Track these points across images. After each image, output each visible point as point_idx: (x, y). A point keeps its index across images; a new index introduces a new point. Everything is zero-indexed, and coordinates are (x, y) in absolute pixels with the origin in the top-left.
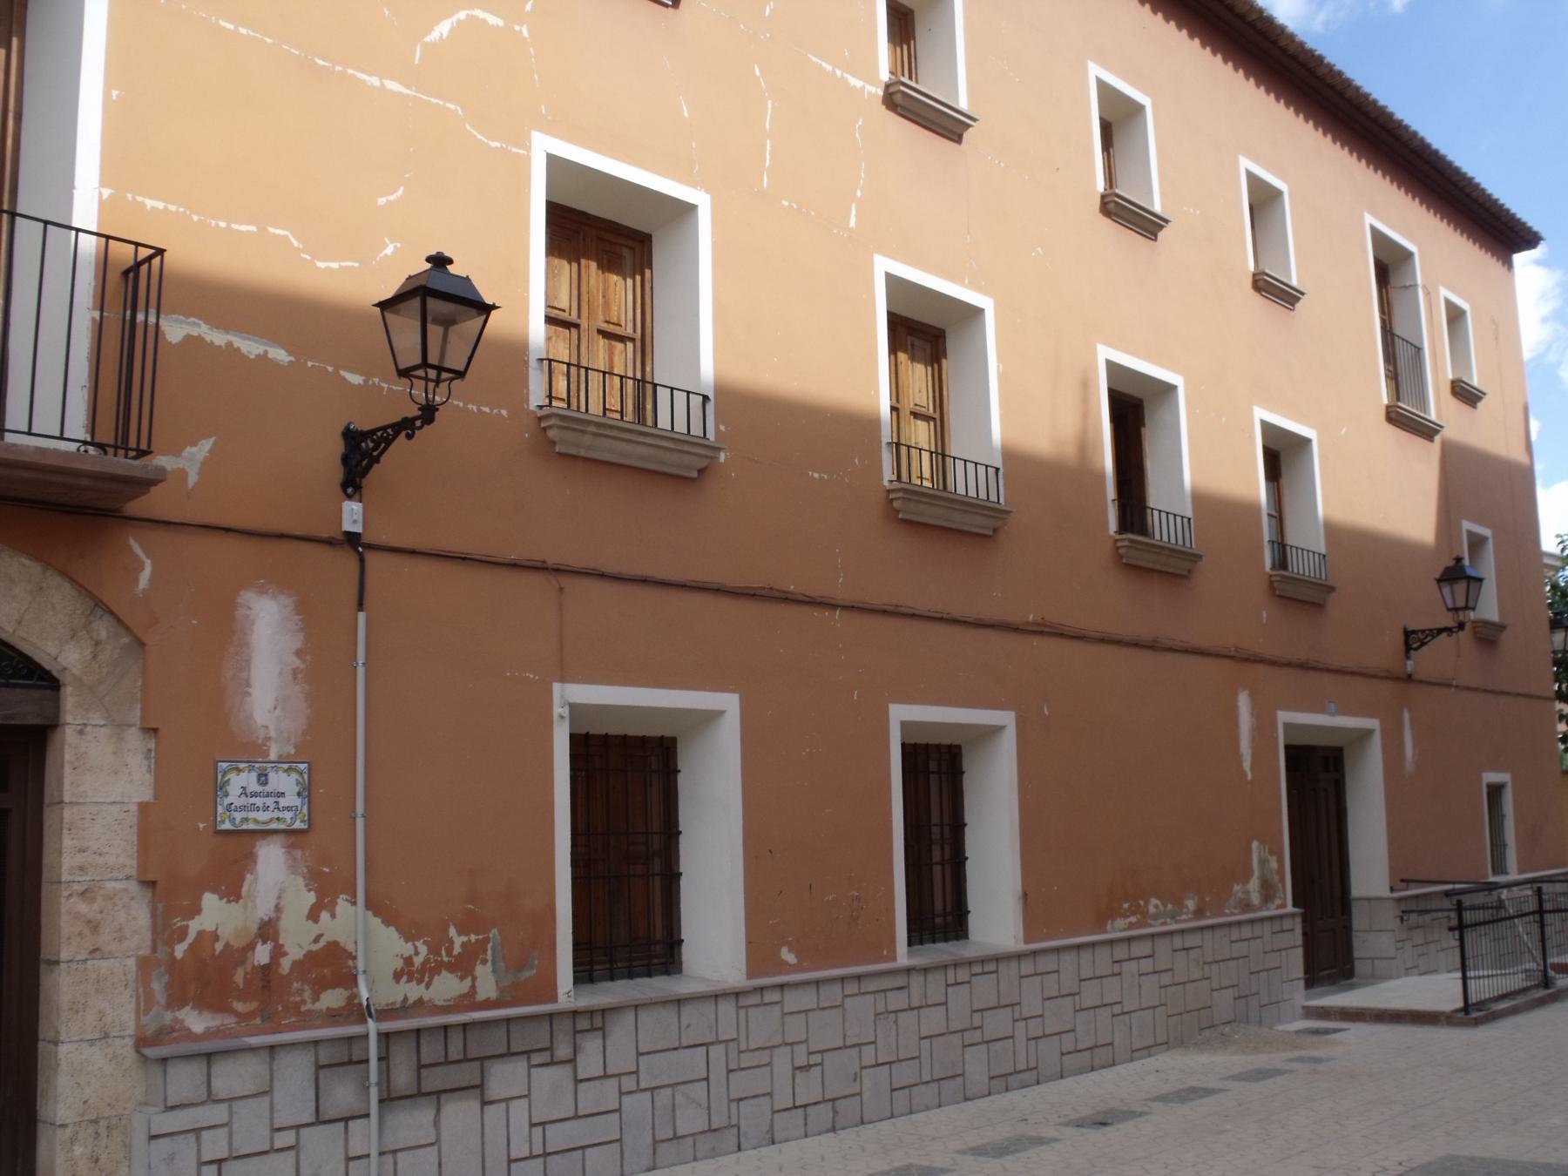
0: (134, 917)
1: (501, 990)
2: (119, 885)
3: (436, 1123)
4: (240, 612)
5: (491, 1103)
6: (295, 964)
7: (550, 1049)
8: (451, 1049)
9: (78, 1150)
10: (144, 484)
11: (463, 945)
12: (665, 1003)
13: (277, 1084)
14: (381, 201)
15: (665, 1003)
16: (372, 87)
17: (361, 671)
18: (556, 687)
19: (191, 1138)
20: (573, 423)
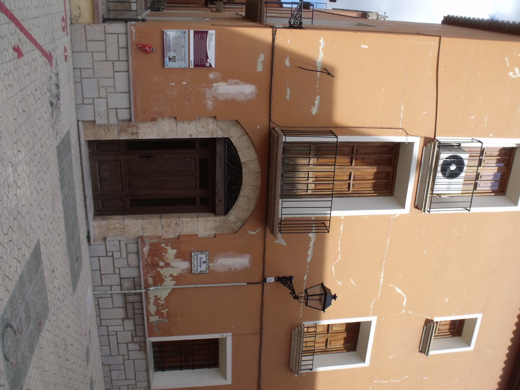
0: (171, 235)
1: (152, 322)
2: (178, 231)
3: (118, 307)
4: (244, 255)
5: (123, 321)
6: (159, 272)
7: (136, 336)
8: (137, 311)
9: (118, 225)
10: (272, 232)
11: (163, 313)
12: (147, 367)
13: (130, 268)
14: (352, 280)
15: (147, 367)
16: (380, 275)
17: (232, 284)
18: (231, 334)
19: (119, 250)
20: (300, 334)
